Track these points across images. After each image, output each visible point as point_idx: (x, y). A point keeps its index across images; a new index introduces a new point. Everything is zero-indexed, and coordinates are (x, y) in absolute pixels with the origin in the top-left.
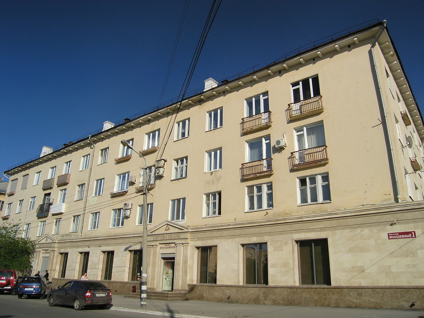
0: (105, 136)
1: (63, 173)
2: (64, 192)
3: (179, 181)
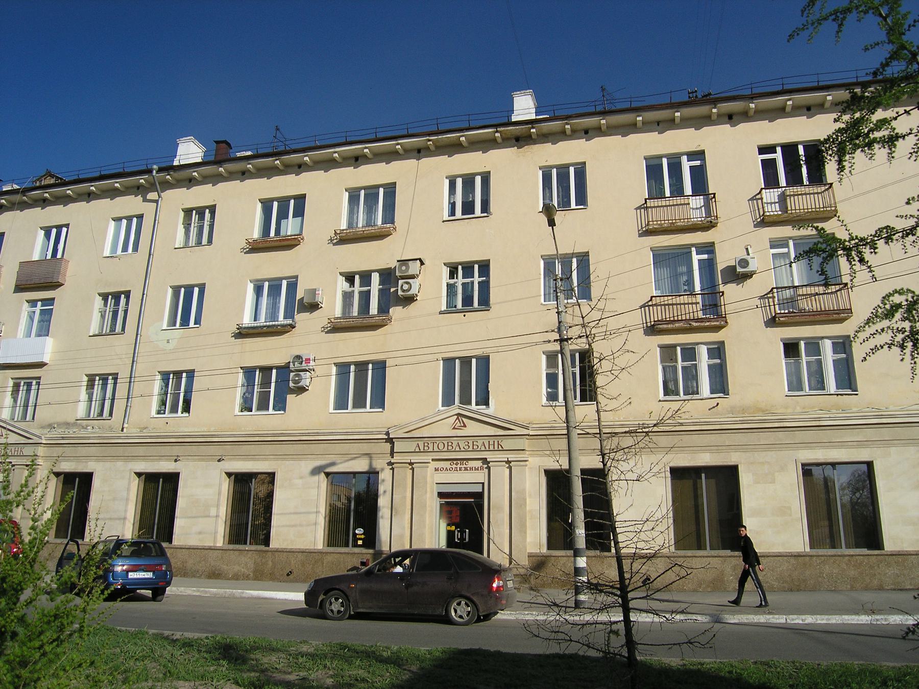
0: (201, 175)
1: (36, 257)
2: (42, 306)
3: (464, 316)
